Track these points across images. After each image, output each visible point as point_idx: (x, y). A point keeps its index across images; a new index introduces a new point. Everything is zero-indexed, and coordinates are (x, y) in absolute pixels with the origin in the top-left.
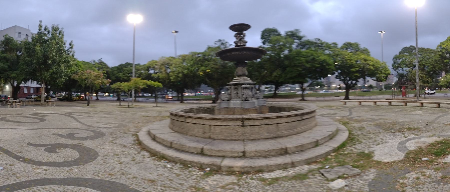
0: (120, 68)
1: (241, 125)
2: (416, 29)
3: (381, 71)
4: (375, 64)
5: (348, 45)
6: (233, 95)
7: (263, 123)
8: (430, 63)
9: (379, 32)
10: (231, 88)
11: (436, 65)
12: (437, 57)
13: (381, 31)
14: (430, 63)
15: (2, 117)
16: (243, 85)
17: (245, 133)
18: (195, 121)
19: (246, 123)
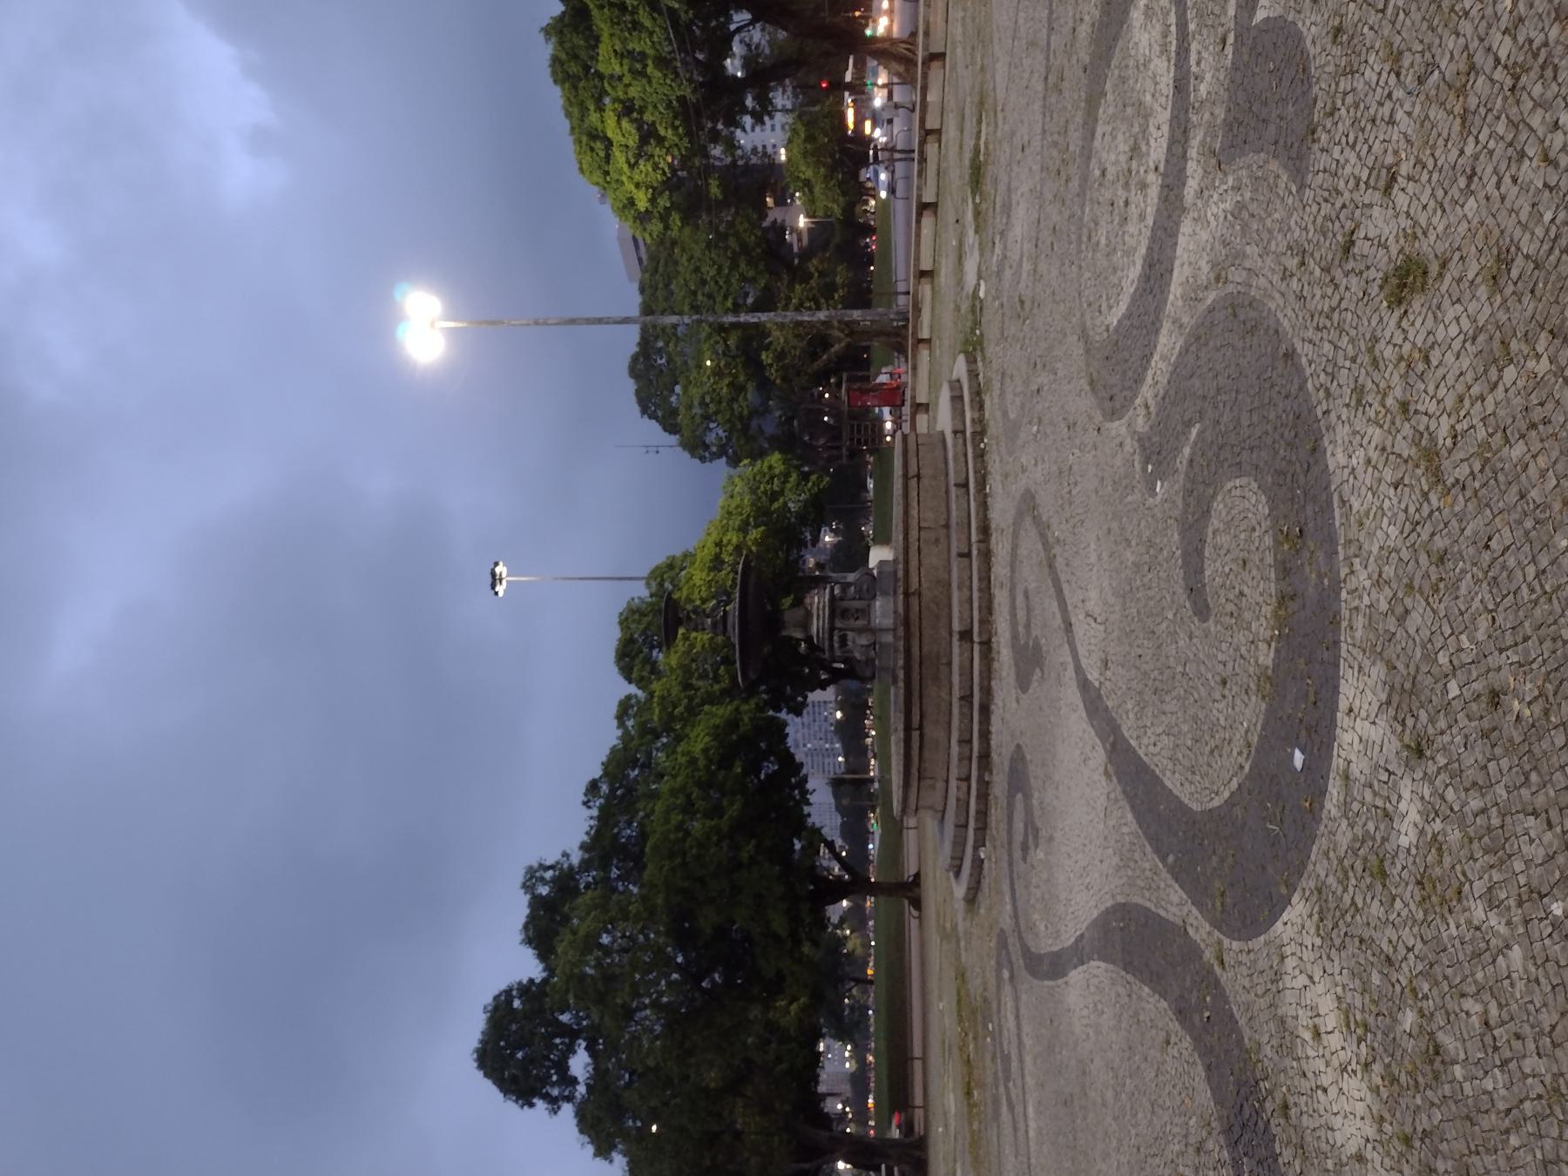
2: (573, 322)
3: (774, 496)
4: (736, 521)
5: (631, 657)
6: (860, 623)
9: (496, 593)
10: (841, 630)
13: (493, 586)
18: (914, 562)
19: (913, 470)
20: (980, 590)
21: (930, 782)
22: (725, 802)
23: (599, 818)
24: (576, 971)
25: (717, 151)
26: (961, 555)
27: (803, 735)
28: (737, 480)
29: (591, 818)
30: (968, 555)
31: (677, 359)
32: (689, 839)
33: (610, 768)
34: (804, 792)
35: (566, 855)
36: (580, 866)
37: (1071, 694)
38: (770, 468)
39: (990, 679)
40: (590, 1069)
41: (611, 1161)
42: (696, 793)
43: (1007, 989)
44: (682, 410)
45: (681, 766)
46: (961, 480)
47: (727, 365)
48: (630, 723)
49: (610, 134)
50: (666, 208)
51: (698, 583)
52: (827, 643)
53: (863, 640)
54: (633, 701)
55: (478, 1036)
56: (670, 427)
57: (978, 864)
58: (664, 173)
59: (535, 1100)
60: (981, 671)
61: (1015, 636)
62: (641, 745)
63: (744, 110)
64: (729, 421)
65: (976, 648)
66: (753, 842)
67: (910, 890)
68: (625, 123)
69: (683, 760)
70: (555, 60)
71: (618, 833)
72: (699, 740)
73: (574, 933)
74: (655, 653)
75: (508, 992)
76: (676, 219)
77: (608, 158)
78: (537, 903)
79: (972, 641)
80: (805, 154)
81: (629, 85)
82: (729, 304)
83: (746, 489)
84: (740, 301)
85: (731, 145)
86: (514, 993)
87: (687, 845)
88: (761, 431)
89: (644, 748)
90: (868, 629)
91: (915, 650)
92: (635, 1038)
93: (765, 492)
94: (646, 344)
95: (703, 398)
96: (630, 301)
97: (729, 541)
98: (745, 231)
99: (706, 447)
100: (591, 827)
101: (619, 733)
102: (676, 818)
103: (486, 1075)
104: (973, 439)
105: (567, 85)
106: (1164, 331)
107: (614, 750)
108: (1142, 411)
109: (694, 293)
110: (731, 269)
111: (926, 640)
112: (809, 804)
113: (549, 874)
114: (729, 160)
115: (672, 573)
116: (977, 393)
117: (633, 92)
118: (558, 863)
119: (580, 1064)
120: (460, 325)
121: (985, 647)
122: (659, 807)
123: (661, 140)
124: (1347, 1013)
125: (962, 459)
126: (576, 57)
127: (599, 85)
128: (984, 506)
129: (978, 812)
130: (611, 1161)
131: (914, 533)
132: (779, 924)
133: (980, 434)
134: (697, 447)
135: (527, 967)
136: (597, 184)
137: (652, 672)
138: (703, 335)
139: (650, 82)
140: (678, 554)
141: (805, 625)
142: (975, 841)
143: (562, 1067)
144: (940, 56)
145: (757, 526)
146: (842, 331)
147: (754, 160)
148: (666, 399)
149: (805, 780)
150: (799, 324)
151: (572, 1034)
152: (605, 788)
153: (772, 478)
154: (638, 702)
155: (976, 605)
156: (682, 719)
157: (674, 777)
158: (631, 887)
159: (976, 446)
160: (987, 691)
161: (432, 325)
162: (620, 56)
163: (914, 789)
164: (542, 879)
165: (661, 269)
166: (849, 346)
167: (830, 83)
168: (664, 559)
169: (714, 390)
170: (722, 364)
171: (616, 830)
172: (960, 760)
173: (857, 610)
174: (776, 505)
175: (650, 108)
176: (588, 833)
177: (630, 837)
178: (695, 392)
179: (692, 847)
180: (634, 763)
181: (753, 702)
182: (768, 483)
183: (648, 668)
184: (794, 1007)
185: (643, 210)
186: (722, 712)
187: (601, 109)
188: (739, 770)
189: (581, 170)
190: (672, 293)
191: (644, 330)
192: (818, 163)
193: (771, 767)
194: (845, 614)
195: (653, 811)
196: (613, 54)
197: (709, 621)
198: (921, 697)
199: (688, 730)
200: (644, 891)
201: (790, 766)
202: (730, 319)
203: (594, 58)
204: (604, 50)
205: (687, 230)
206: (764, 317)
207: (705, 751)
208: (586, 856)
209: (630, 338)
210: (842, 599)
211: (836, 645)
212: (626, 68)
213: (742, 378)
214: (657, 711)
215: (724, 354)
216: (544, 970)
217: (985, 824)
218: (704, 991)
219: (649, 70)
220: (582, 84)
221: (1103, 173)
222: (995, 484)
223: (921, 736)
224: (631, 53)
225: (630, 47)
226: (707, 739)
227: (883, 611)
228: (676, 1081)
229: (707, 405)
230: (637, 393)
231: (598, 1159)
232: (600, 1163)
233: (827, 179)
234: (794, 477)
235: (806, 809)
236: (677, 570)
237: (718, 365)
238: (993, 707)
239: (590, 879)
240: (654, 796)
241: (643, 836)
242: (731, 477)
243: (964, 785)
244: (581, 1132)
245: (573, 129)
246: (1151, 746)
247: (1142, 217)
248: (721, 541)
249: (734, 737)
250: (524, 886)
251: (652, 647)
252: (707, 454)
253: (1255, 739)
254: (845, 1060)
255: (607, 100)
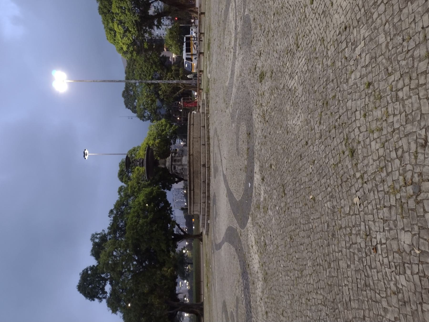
2: (104, 81)
3: (163, 131)
4: (152, 138)
5: (122, 175)
6: (179, 163)
8: (149, 68)
9: (85, 158)
10: (174, 165)
11: (151, 61)
12: (140, 59)
13: (84, 156)
14: (149, 68)
19: (192, 123)
20: (207, 153)
21: (196, 204)
22: (148, 215)
23: (113, 220)
24: (106, 262)
25: (147, 35)
26: (203, 145)
27: (175, 198)
28: (152, 126)
29: (111, 220)
30: (205, 145)
31: (136, 92)
32: (138, 225)
33: (116, 206)
34: (171, 211)
35: (103, 231)
36: (108, 234)
37: (222, 178)
38: (162, 123)
39: (210, 176)
40: (111, 289)
41: (117, 314)
42: (140, 212)
43: (213, 255)
44: (137, 107)
45: (136, 205)
46: (203, 126)
47: (150, 94)
48: (122, 194)
49: (115, 29)
50: (132, 50)
51: (142, 154)
52: (170, 169)
53: (180, 168)
54: (123, 187)
55: (78, 282)
56: (134, 111)
57: (208, 225)
58: (131, 41)
59: (95, 299)
60: (207, 175)
61: (214, 165)
62: (125, 199)
63: (154, 25)
64: (151, 110)
65: (207, 168)
66: (156, 225)
67: (200, 237)
68: (120, 26)
69: (137, 203)
70: (100, 8)
71: (119, 224)
72: (141, 197)
73: (105, 252)
74: (129, 174)
75: (87, 269)
76: (135, 53)
77: (115, 36)
78: (95, 244)
79: (206, 167)
80: (170, 37)
81: (121, 16)
82: (150, 77)
83: (155, 128)
84: (154, 77)
85: (150, 34)
86: (89, 269)
87: (138, 226)
88: (160, 113)
89: (126, 200)
90: (181, 165)
91: (192, 170)
92: (124, 280)
93: (160, 130)
94: (127, 88)
95: (143, 103)
96: (123, 77)
97: (150, 143)
98: (155, 57)
99: (145, 117)
100: (111, 223)
101: (119, 196)
102: (134, 219)
103: (80, 293)
104: (206, 115)
105: (103, 15)
106: (234, 88)
107: (118, 201)
108: (231, 107)
109: (141, 74)
110: (151, 68)
111: (194, 167)
112: (172, 214)
113: (98, 236)
114: (150, 38)
115: (134, 152)
116: (208, 103)
117: (122, 18)
118: (101, 233)
119: (108, 288)
120: (72, 81)
121: (208, 168)
122: (130, 216)
123: (130, 32)
124: (255, 240)
125: (204, 120)
126: (106, 7)
127: (112, 15)
128: (208, 132)
129: (207, 211)
130: (117, 314)
131: (192, 139)
132: (163, 247)
133: (208, 113)
134: (142, 117)
135: (92, 262)
136: (112, 43)
137: (128, 179)
138: (143, 86)
139: (127, 15)
140: (136, 146)
141: (165, 164)
142: (207, 219)
143: (103, 289)
144: (204, 13)
145: (158, 139)
146: (182, 86)
147: (157, 38)
148: (133, 104)
149: (171, 208)
150: (169, 84)
151: (105, 280)
152: (115, 212)
153: (162, 126)
154: (125, 187)
155: (206, 157)
156: (137, 192)
157: (134, 208)
158: (122, 239)
159: (207, 116)
160: (209, 180)
161: (63, 81)
162: (118, 8)
163: (192, 206)
164: (97, 238)
165: (131, 67)
166: (184, 90)
167: (178, 18)
168: (132, 148)
169: (146, 101)
170: (149, 94)
171: (118, 223)
172: (203, 198)
173: (178, 160)
174: (163, 133)
175: (127, 23)
176: (110, 224)
177: (122, 225)
178: (141, 102)
179: (139, 227)
180: (123, 205)
181: (157, 187)
182: (161, 127)
183: (127, 178)
184: (169, 270)
185: (125, 51)
186: (148, 190)
187: (113, 22)
188: (153, 206)
189: (107, 39)
190: (134, 74)
191: (126, 84)
192: (173, 40)
193: (162, 205)
194: (175, 161)
195: (128, 218)
196: (116, 7)
197: (138, 163)
198: (193, 182)
199: (138, 195)
200: (126, 240)
201: (167, 204)
202: (150, 82)
203: (111, 8)
204: (113, 6)
205: (138, 57)
206: (159, 81)
207: (143, 200)
208: (110, 231)
209: (122, 87)
210: (174, 157)
211: (173, 169)
212: (120, 11)
213: (154, 98)
214: (130, 190)
215: (149, 91)
216: (97, 263)
217: (209, 214)
218: (143, 267)
219: (126, 12)
220: (107, 15)
221: (226, 48)
222: (211, 127)
223: (194, 192)
224: (122, 7)
225: (121, 5)
226: (144, 197)
227: (185, 160)
228: (135, 291)
229: (145, 105)
230: (125, 102)
231: (113, 314)
232: (114, 315)
233: (175, 44)
234: (168, 126)
235: (172, 216)
236: (136, 151)
237: (147, 94)
238: (210, 184)
239: (111, 237)
240: (128, 213)
241: (126, 224)
242: (151, 125)
243: (204, 204)
244: (108, 307)
245: (105, 27)
246: (232, 189)
247: (231, 59)
248: (148, 143)
249: (151, 197)
250: (91, 239)
251: (129, 172)
252: (145, 119)
253: (245, 182)
254: (187, 286)
255: (115, 20)
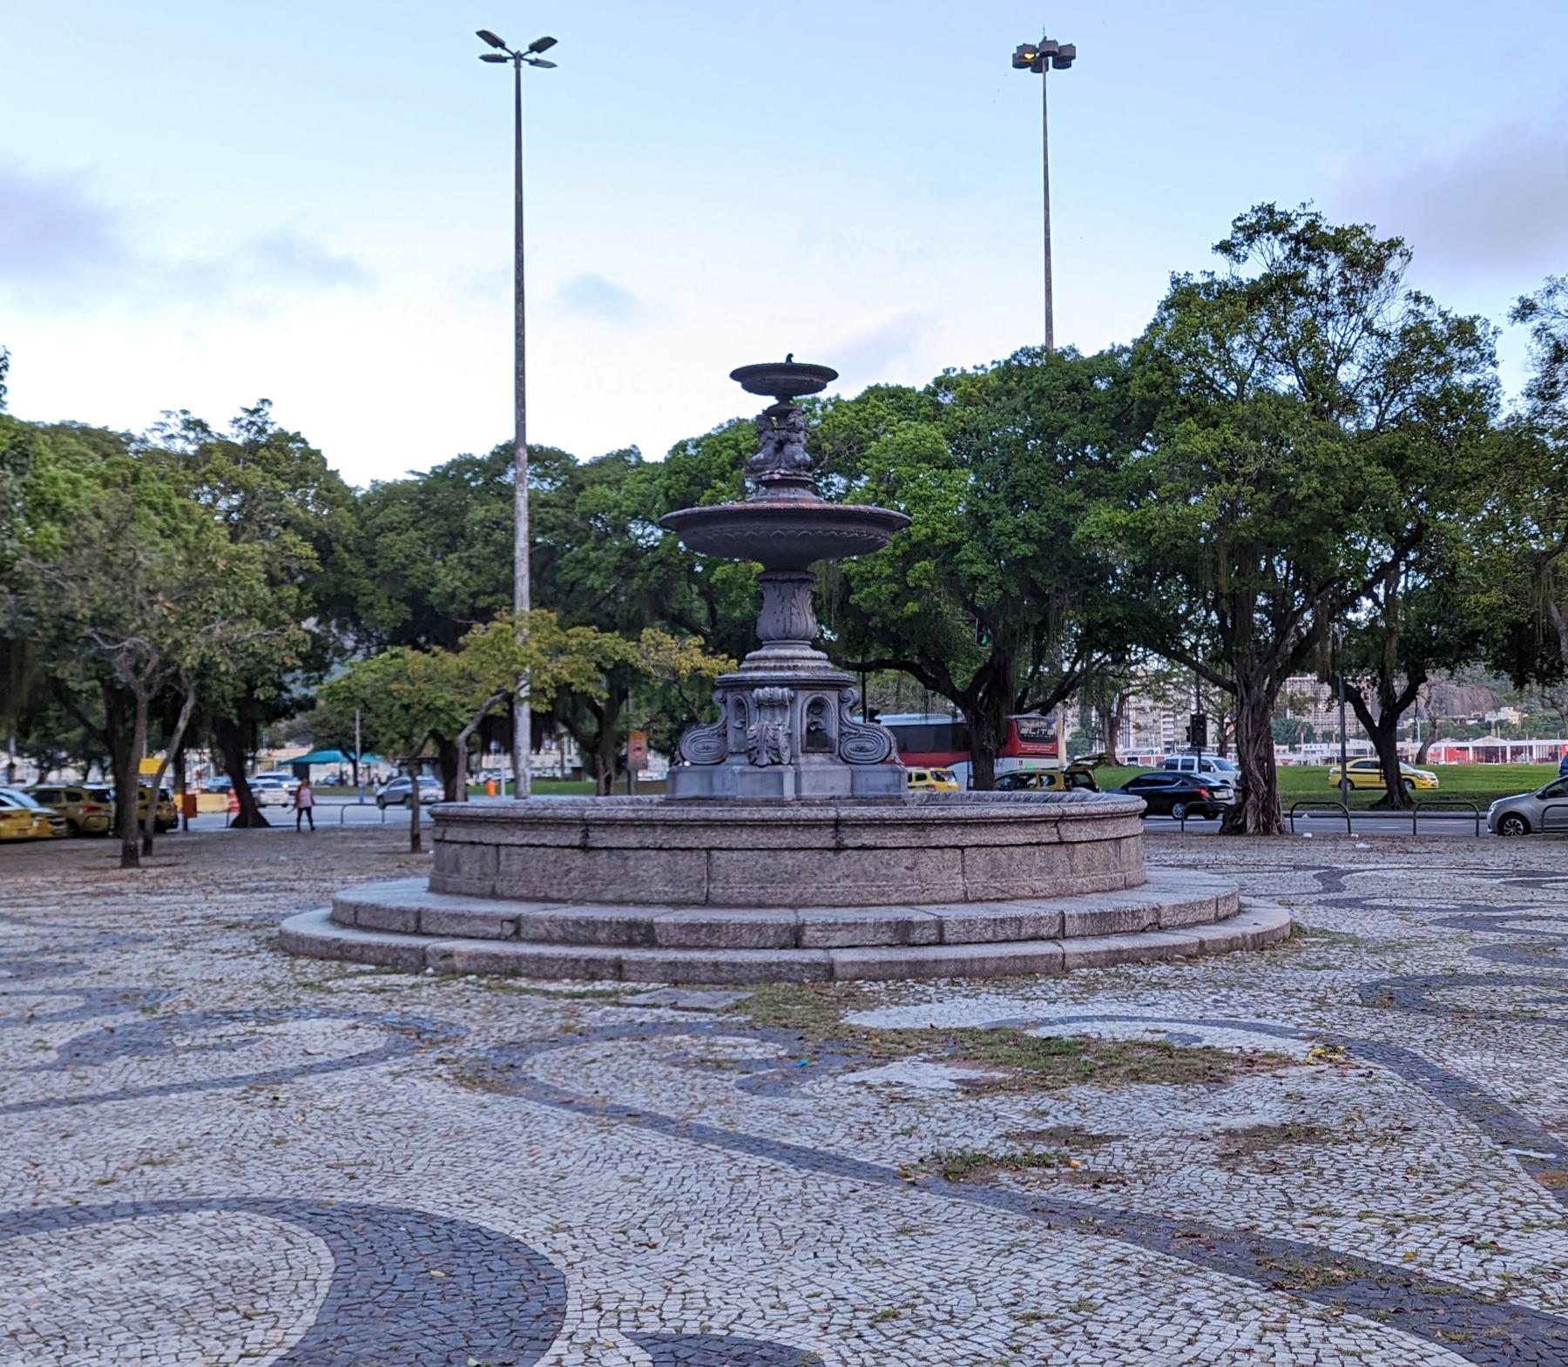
0: (444, 496)
1: (577, 842)
7: (649, 841)
10: (793, 700)
15: (3, 960)
16: (762, 687)
17: (592, 877)
19: (599, 838)
